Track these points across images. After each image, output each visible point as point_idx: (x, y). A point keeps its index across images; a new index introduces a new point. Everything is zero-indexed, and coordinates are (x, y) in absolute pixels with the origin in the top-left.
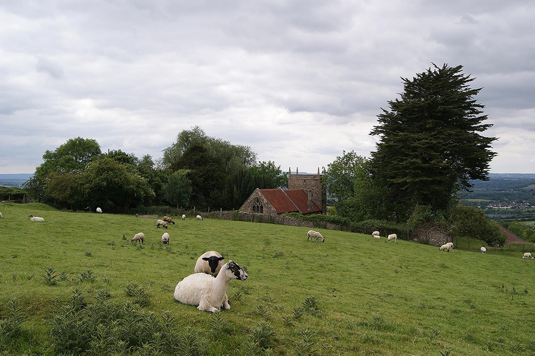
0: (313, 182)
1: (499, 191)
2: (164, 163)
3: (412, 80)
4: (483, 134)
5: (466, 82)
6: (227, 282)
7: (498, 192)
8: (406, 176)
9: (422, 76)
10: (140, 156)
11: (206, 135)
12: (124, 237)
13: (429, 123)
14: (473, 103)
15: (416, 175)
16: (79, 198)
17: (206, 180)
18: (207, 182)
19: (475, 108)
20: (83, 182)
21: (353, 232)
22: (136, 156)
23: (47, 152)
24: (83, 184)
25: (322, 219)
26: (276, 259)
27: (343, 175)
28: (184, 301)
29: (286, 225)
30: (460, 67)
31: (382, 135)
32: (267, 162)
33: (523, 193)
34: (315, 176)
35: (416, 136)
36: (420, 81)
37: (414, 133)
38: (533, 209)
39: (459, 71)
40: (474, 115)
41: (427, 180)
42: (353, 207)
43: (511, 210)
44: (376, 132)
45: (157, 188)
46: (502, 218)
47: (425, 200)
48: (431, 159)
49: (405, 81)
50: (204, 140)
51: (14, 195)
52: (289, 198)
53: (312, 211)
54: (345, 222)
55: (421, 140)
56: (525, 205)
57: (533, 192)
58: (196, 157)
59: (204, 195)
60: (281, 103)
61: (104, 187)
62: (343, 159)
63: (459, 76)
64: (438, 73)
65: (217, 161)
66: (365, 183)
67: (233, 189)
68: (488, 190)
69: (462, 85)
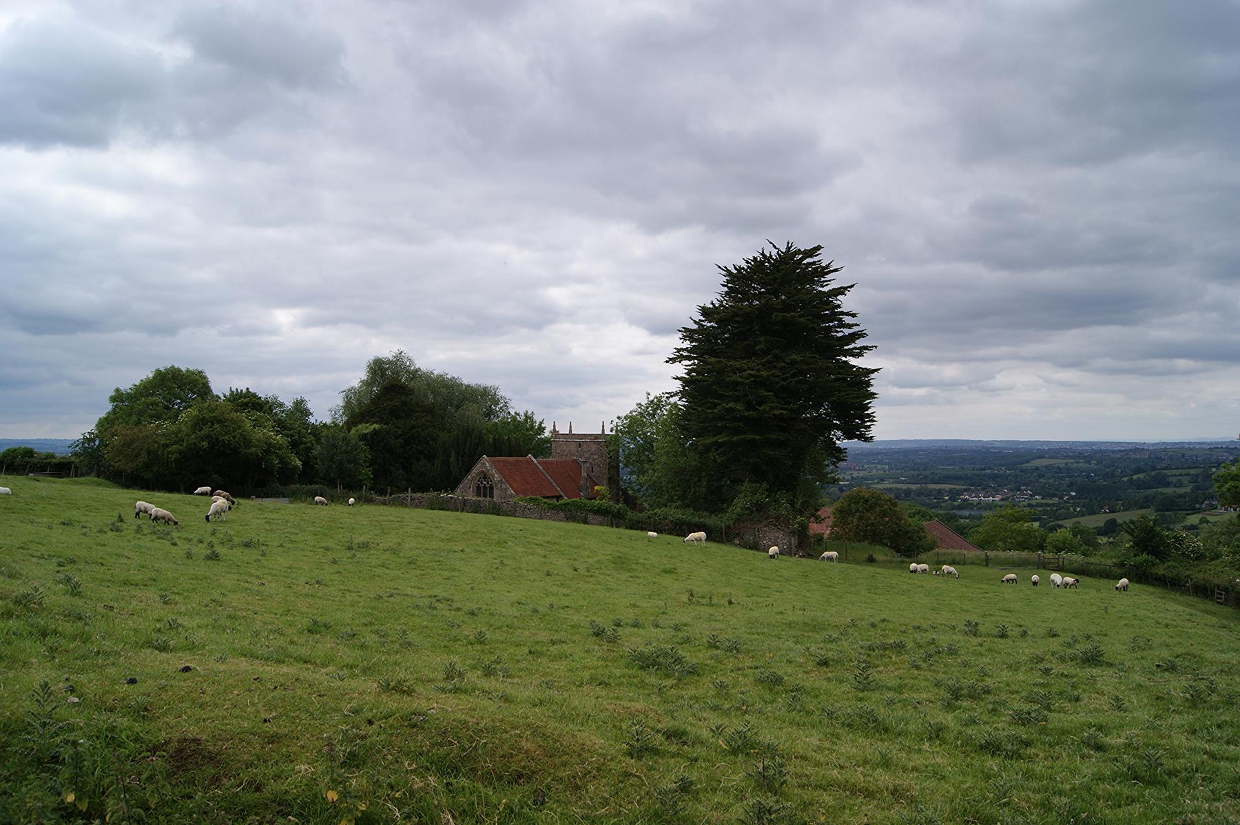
0: (594, 447)
1: (982, 470)
3: (739, 269)
9: (753, 263)
16: (161, 470)
18: (409, 447)
20: (168, 442)
21: (631, 529)
22: (280, 399)
23: (117, 390)
24: (167, 446)
29: (518, 517)
30: (819, 248)
32: (522, 413)
33: (1022, 474)
34: (596, 436)
35: (736, 364)
37: (735, 359)
38: (1036, 501)
39: (816, 256)
40: (842, 329)
43: (1000, 503)
49: (723, 270)
50: (415, 374)
51: (55, 464)
52: (546, 474)
54: (619, 512)
57: (1038, 471)
65: (430, 410)
68: (963, 469)
69: (823, 279)
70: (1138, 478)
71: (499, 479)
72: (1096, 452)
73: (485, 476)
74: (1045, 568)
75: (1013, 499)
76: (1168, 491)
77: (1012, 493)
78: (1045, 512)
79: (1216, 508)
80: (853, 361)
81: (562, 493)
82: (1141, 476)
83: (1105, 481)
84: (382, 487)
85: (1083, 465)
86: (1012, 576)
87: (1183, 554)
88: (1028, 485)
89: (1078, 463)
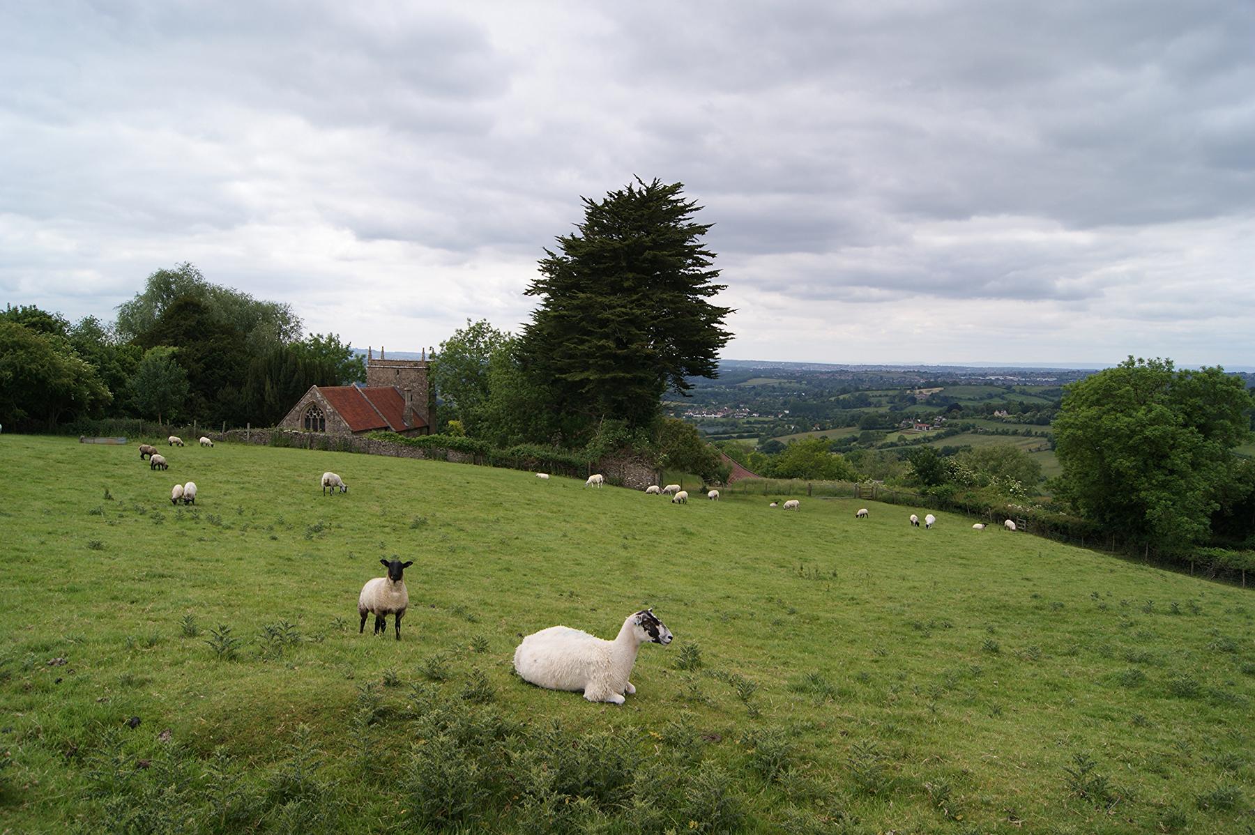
0: (413, 375)
2: (120, 331)
3: (600, 203)
4: (712, 301)
5: (687, 212)
6: (638, 646)
7: (701, 390)
8: (587, 369)
9: (616, 197)
10: (74, 317)
11: (206, 280)
12: (107, 493)
13: (627, 279)
14: (699, 249)
15: (604, 369)
17: (208, 367)
18: (210, 372)
19: (700, 256)
22: (65, 318)
25: (440, 444)
26: (417, 531)
27: (469, 364)
28: (551, 684)
29: (373, 454)
30: (679, 185)
31: (545, 295)
32: (326, 336)
34: (416, 363)
35: (606, 300)
36: (613, 204)
37: (601, 294)
41: (623, 377)
42: (487, 421)
43: (722, 420)
44: (536, 289)
45: (115, 382)
46: (707, 434)
47: (618, 411)
48: (631, 341)
50: (202, 289)
53: (413, 427)
54: (481, 448)
55: (614, 307)
56: (743, 412)
58: (188, 322)
59: (206, 395)
60: (342, 222)
61: (7, 381)
62: (468, 334)
63: (677, 201)
64: (645, 193)
65: (228, 331)
66: (512, 379)
67: (264, 385)
69: (680, 217)
70: (844, 398)
71: (332, 410)
72: (806, 372)
73: (315, 407)
74: (860, 497)
75: (733, 417)
76: (871, 410)
77: (732, 411)
78: (763, 429)
79: (912, 427)
80: (710, 301)
81: (389, 424)
82: (846, 396)
83: (815, 400)
84: (184, 416)
85: (795, 385)
86: (864, 510)
87: (958, 481)
88: (746, 403)
89: (790, 383)
